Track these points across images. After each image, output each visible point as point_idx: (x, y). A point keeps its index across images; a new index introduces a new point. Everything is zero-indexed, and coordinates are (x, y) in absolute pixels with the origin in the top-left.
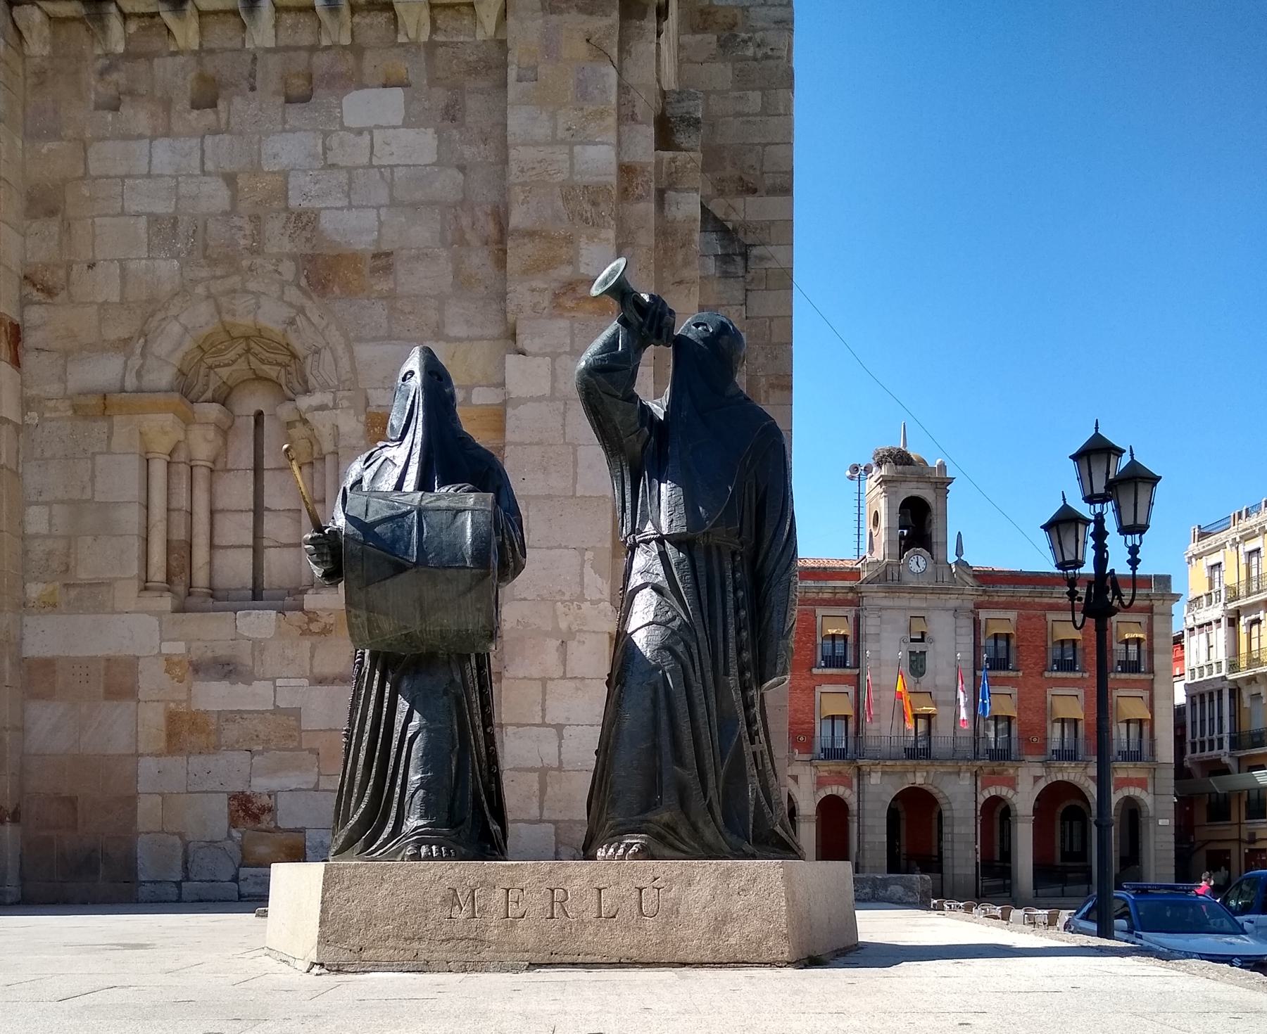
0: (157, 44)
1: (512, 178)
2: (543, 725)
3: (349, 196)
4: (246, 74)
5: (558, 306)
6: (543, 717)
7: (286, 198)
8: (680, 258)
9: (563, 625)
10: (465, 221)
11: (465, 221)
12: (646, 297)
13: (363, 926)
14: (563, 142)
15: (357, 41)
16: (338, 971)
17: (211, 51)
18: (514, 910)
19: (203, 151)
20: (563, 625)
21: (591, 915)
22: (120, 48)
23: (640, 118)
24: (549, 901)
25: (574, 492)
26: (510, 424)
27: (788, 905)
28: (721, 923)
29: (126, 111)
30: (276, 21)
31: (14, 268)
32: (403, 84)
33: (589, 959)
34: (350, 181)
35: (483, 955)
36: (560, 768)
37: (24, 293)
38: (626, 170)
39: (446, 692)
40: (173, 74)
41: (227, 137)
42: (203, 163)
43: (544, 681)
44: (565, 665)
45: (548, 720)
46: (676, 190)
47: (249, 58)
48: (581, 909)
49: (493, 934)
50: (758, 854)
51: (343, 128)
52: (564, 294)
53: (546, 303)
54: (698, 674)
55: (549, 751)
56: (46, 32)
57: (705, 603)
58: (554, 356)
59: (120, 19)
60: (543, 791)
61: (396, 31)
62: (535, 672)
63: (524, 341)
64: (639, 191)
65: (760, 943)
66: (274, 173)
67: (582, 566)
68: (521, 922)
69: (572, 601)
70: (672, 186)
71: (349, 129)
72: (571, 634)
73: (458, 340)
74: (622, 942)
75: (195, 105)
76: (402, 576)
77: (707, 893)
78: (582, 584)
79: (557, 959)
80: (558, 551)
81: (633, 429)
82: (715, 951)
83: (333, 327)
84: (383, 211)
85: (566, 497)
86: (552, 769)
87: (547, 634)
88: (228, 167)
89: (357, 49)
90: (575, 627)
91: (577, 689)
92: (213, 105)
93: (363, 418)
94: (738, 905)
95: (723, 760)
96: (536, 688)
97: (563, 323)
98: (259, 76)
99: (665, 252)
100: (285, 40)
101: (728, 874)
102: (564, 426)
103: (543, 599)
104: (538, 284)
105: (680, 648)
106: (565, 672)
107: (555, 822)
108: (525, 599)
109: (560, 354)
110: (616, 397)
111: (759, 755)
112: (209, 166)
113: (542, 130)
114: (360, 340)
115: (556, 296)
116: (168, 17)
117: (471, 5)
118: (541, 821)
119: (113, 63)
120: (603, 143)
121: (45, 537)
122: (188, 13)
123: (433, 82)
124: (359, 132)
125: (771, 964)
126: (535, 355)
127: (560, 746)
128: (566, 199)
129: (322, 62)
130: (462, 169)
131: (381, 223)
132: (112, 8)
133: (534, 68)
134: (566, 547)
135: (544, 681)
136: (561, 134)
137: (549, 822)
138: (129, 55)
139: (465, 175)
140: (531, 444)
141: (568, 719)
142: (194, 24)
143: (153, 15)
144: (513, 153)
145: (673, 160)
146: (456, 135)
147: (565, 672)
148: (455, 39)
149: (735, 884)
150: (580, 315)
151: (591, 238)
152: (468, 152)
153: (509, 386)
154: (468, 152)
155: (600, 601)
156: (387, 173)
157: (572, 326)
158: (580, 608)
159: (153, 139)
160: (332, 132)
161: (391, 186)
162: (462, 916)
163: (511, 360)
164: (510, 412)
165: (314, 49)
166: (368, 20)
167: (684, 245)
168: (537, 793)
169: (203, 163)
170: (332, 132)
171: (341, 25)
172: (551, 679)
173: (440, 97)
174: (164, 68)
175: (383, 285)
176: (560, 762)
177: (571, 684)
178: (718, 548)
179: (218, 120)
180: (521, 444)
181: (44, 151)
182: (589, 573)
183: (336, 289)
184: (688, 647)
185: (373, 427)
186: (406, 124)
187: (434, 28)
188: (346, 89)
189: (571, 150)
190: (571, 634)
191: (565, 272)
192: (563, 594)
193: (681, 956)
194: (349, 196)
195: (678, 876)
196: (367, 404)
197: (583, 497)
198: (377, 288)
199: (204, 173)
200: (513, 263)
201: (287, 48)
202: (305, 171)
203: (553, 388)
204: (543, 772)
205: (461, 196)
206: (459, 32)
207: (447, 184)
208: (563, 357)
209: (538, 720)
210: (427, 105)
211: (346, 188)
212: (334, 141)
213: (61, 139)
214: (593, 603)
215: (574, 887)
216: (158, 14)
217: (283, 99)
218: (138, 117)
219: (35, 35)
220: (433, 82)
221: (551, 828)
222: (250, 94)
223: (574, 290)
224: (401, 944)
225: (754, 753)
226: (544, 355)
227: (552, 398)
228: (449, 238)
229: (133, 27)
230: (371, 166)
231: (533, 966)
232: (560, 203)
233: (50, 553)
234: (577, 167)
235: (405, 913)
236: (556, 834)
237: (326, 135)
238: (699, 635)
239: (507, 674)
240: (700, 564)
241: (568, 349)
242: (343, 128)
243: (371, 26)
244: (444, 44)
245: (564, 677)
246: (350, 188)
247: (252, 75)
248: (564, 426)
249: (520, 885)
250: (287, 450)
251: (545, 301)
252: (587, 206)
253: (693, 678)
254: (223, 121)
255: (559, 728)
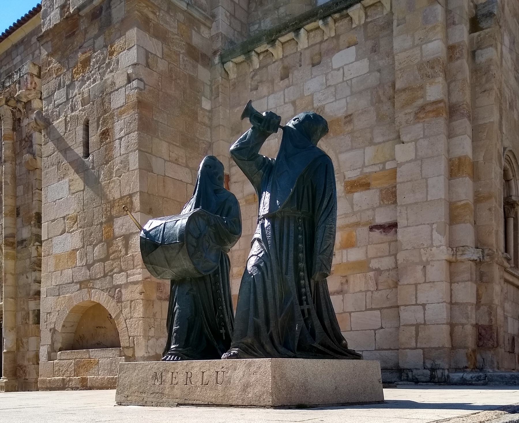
0: (269, 60)
1: (396, 68)
2: (417, 304)
3: (335, 96)
4: (298, 61)
5: (418, 118)
6: (416, 301)
7: (313, 104)
8: (484, 79)
9: (424, 259)
10: (381, 93)
11: (381, 93)
12: (264, 114)
13: (128, 387)
14: (417, 45)
15: (337, 33)
16: (120, 405)
17: (287, 56)
18: (174, 382)
19: (284, 95)
20: (424, 259)
21: (199, 384)
22: (258, 67)
23: (457, 22)
24: (186, 377)
25: (427, 199)
26: (398, 175)
27: (272, 379)
28: (246, 387)
29: (260, 89)
30: (308, 37)
31: (226, 155)
32: (355, 44)
33: (198, 402)
34: (336, 90)
35: (163, 399)
36: (425, 324)
37: (231, 163)
38: (451, 49)
39: (187, 294)
40: (275, 69)
41: (292, 87)
42: (284, 99)
43: (416, 285)
44: (425, 277)
45: (418, 302)
46: (481, 49)
47: (299, 54)
48: (196, 381)
49: (167, 391)
50: (242, 356)
51: (333, 70)
52: (420, 112)
53: (412, 118)
54: (270, 275)
55: (420, 316)
56: (235, 69)
57: (278, 243)
58: (416, 141)
59: (257, 56)
60: (417, 334)
61: (352, 23)
62: (412, 281)
63: (404, 138)
64: (458, 55)
65: (260, 397)
66: (308, 96)
67: (432, 231)
68: (176, 386)
69: (428, 248)
70: (479, 48)
71: (335, 69)
72: (428, 262)
73: (379, 143)
74: (210, 395)
75: (282, 79)
76: (158, 249)
77: (241, 374)
78: (432, 239)
79: (187, 402)
80: (420, 227)
81: (255, 172)
82: (243, 400)
83: (331, 150)
84: (348, 98)
85: (423, 202)
86: (421, 324)
87: (417, 264)
88: (292, 98)
89: (337, 37)
90: (429, 259)
91: (431, 287)
92: (287, 77)
93: (343, 184)
94: (253, 379)
95: (281, 314)
96: (412, 289)
97: (420, 125)
98: (303, 59)
99: (477, 78)
100: (311, 43)
101: (249, 365)
102: (421, 171)
103: (415, 248)
104: (408, 110)
105: (262, 265)
106: (425, 280)
107: (423, 349)
108: (407, 249)
109: (419, 139)
110: (244, 160)
111: (306, 312)
112: (287, 100)
113: (408, 44)
114: (341, 153)
115: (416, 114)
116: (271, 50)
117: (380, 2)
118: (416, 348)
119: (256, 72)
120: (435, 40)
121: (238, 250)
122: (277, 45)
123: (367, 38)
124: (338, 69)
125: (264, 407)
126: (408, 142)
127: (424, 314)
128: (419, 70)
129: (325, 46)
130: (379, 71)
131: (347, 103)
132: (253, 53)
133: (404, 18)
134: (424, 224)
135: (416, 285)
136: (417, 42)
137: (420, 348)
138: (261, 68)
139: (380, 73)
140: (407, 181)
141: (427, 301)
142: (280, 49)
143: (267, 51)
144: (396, 57)
145: (479, 35)
146: (376, 57)
147: (425, 280)
148: (375, 18)
149: (253, 369)
150: (427, 120)
151: (431, 84)
152: (381, 63)
153: (397, 159)
154: (381, 63)
155: (440, 246)
156: (349, 82)
157: (424, 126)
158: (431, 250)
159: (268, 96)
160: (328, 73)
161: (351, 87)
162: (158, 384)
163: (398, 147)
164: (398, 169)
165: (321, 42)
166: (341, 23)
167: (486, 73)
168: (415, 335)
169: (284, 99)
170: (328, 73)
171: (330, 29)
172: (420, 284)
173: (370, 44)
174: (272, 68)
175: (349, 128)
176: (425, 320)
177: (428, 285)
178: (288, 217)
179: (289, 82)
180: (403, 182)
181: (236, 111)
182: (435, 234)
183: (331, 135)
184: (265, 264)
185: (347, 187)
186: (357, 60)
187: (367, 16)
188: (333, 54)
189: (421, 48)
190: (428, 262)
191: (420, 102)
192: (424, 245)
193: (230, 402)
194: (335, 96)
195: (231, 366)
196: (345, 178)
197: (431, 200)
198: (347, 130)
199: (285, 103)
200: (397, 105)
201: (312, 45)
202: (319, 91)
203: (416, 155)
204: (417, 326)
205: (378, 83)
206: (376, 14)
207: (373, 79)
208: (420, 140)
209: (414, 303)
210: (364, 49)
211: (334, 93)
212: (329, 76)
213: (241, 105)
214: (437, 247)
215: (195, 371)
216: (267, 51)
217: (311, 66)
218: (264, 89)
219: (231, 72)
220: (367, 38)
221: (421, 351)
222: (299, 68)
223: (424, 109)
224: (139, 395)
225: (303, 311)
226: (411, 141)
227: (416, 159)
228: (374, 101)
229: (261, 57)
230: (343, 81)
231: (179, 405)
232: (417, 73)
233: (240, 256)
234: (424, 54)
235: (141, 382)
236: (424, 354)
237: (326, 74)
238: (272, 258)
239: (400, 283)
240: (277, 226)
241: (422, 136)
242: (333, 70)
243: (342, 25)
244: (371, 22)
245: (425, 282)
246: (336, 93)
247: (300, 61)
248: (421, 171)
249: (176, 371)
250: (124, 208)
251: (412, 117)
252: (429, 70)
253: (266, 277)
254: (291, 81)
255: (424, 305)
